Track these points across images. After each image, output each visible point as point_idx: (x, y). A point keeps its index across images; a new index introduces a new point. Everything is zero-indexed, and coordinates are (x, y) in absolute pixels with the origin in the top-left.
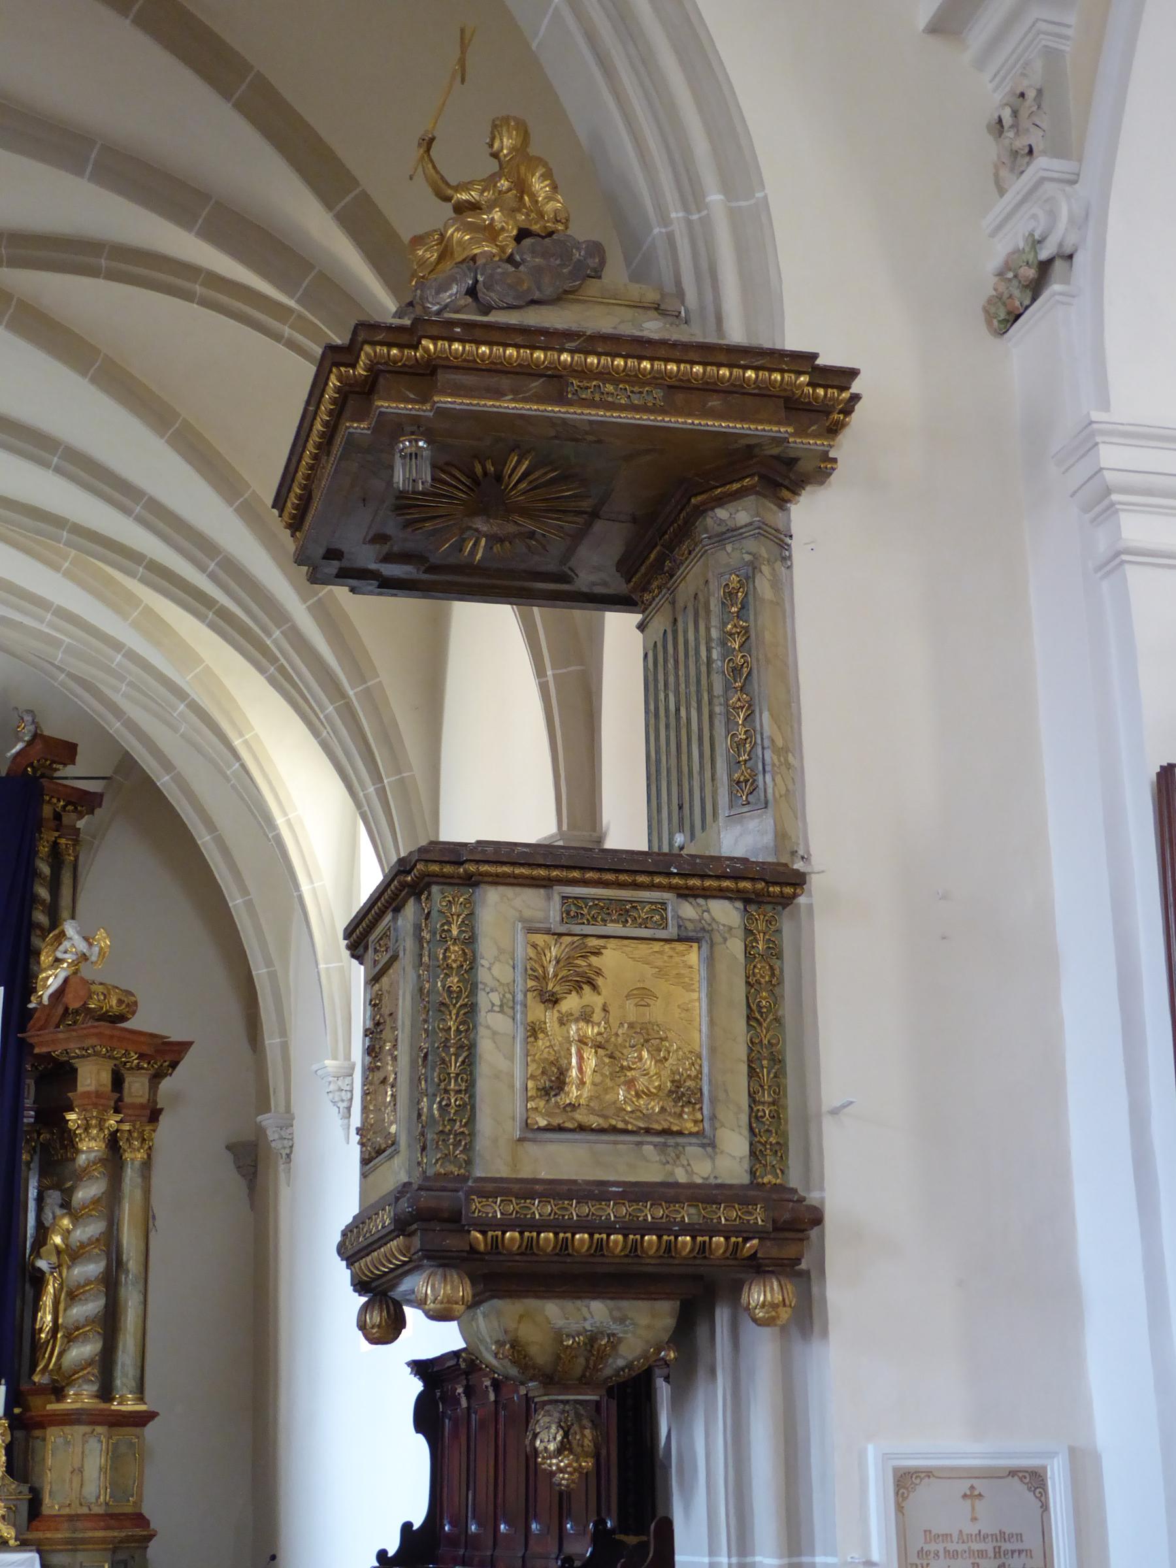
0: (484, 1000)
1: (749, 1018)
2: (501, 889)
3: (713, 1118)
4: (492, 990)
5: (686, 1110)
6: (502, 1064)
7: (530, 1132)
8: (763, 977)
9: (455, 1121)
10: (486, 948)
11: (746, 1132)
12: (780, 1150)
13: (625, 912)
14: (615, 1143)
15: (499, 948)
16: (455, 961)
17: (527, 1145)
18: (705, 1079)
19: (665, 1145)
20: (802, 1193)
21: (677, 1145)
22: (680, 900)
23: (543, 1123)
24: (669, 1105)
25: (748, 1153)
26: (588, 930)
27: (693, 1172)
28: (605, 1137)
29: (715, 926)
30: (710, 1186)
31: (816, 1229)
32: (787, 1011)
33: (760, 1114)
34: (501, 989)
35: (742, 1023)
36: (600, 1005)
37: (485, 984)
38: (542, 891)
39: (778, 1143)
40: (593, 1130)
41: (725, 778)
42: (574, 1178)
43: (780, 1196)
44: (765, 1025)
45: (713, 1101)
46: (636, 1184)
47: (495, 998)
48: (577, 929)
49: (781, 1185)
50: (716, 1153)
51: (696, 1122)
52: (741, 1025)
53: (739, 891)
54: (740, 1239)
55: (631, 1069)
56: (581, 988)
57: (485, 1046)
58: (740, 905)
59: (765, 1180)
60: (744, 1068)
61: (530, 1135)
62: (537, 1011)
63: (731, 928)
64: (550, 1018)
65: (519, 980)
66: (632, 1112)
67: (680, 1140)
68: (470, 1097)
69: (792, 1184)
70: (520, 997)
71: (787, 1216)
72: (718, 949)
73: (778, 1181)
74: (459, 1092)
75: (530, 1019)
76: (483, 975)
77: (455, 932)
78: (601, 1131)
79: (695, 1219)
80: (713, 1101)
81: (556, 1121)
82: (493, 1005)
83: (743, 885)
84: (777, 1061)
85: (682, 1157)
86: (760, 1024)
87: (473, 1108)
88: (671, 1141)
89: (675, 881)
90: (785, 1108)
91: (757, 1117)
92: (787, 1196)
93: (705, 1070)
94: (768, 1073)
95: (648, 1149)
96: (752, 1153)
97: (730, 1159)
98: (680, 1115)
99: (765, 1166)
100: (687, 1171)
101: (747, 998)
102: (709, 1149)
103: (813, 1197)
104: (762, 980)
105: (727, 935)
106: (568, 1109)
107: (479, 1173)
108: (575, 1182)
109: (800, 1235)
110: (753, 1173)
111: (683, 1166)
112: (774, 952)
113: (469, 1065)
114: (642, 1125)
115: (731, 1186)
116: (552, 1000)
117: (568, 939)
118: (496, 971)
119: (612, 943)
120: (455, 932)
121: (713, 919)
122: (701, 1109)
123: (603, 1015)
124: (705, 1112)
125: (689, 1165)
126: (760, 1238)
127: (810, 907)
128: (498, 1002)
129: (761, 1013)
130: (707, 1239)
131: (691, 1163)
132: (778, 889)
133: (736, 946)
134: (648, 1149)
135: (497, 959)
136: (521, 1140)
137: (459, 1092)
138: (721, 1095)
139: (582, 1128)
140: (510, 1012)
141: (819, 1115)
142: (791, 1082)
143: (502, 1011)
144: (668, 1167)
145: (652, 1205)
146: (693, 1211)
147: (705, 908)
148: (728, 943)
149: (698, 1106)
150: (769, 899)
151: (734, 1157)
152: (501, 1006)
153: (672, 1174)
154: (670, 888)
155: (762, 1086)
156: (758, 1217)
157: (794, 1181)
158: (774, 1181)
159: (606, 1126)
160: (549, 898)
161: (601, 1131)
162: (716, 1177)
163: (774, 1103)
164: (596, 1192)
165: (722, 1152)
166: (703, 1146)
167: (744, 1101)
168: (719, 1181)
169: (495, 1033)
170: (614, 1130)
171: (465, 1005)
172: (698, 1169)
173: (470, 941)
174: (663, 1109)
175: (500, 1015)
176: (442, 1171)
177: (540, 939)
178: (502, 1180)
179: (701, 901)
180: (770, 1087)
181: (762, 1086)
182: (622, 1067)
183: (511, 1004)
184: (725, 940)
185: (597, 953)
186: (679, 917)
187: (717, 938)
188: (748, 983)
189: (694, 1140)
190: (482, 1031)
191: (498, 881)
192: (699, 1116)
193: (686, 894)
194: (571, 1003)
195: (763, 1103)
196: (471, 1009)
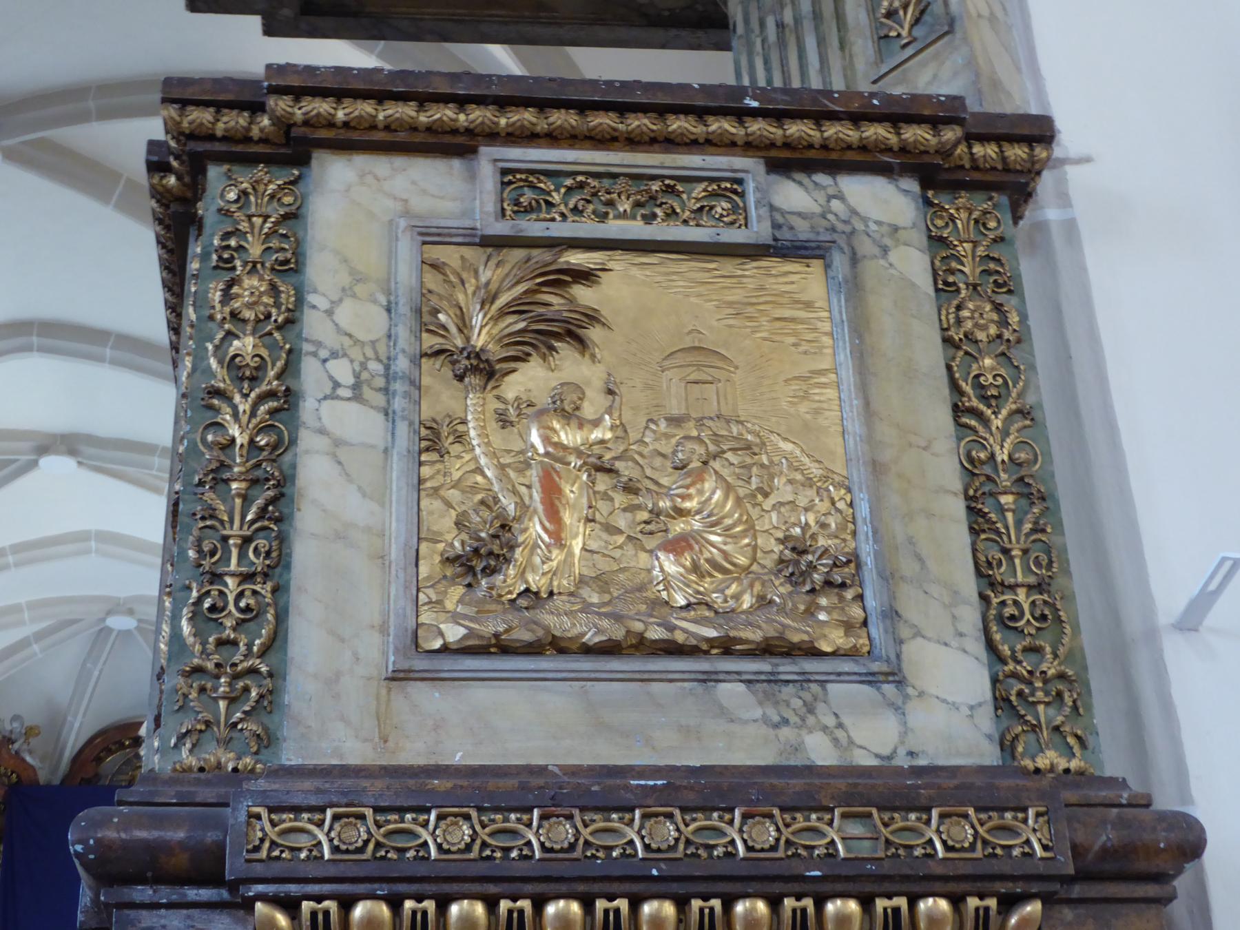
0: (311, 377)
1: (957, 410)
2: (361, 161)
3: (892, 614)
4: (334, 355)
5: (823, 601)
6: (356, 508)
7: (418, 663)
8: (984, 328)
9: (234, 643)
10: (322, 272)
11: (979, 648)
12: (1069, 688)
13: (655, 196)
14: (645, 679)
15: (353, 272)
16: (250, 306)
17: (420, 693)
18: (864, 529)
19: (773, 680)
20: (1135, 786)
21: (805, 680)
22: (774, 177)
23: (454, 633)
24: (780, 590)
25: (988, 695)
26: (561, 230)
27: (851, 742)
28: (615, 664)
29: (860, 226)
30: (899, 771)
31: (1189, 867)
32: (1044, 391)
33: (1009, 611)
34: (356, 353)
35: (942, 417)
36: (598, 383)
37: (319, 344)
38: (456, 163)
39: (1062, 676)
40: (588, 650)
41: (863, 17)
42: (539, 761)
43: (1078, 795)
44: (997, 422)
45: (888, 577)
46: (703, 770)
47: (342, 371)
48: (533, 227)
49: (1081, 773)
50: (907, 697)
51: (848, 627)
52: (937, 417)
53: (904, 150)
54: (992, 903)
55: (681, 513)
56: (552, 348)
57: (315, 471)
58: (912, 185)
59: (1042, 762)
60: (958, 507)
61: (420, 664)
62: (443, 395)
63: (896, 229)
64: (474, 407)
65: (403, 334)
66: (688, 606)
67: (810, 665)
68: (275, 591)
69: (1112, 768)
70: (402, 364)
71: (1108, 837)
72: (872, 269)
73: (1074, 764)
74: (247, 578)
75: (427, 412)
76: (314, 325)
77: (255, 251)
78: (609, 649)
79: (864, 849)
80: (888, 577)
81: (491, 627)
82: (337, 385)
83: (913, 133)
84: (1035, 493)
85: (821, 707)
86: (985, 422)
87: (281, 617)
88: (787, 668)
89: (757, 127)
90: (1069, 598)
91: (1001, 620)
92: (1105, 794)
93: (863, 509)
94: (1019, 523)
95: (731, 692)
96: (1001, 702)
97: (945, 708)
98: (810, 612)
99: (1035, 728)
100: (836, 741)
101: (949, 368)
102: (889, 689)
103: (1165, 801)
104: (981, 336)
105: (887, 241)
106: (523, 602)
107: (290, 756)
108: (542, 770)
109: (1151, 890)
110: (1007, 746)
111: (825, 729)
112: (1000, 284)
113: (278, 521)
114: (712, 633)
115: (953, 771)
116: (483, 370)
117: (519, 254)
118: (346, 314)
119: (619, 263)
120: (255, 251)
121: (854, 212)
122: (860, 597)
123: (605, 401)
124: (871, 602)
125: (840, 725)
126: (1048, 900)
127: (1071, 227)
128: (347, 379)
129: (984, 399)
130: (902, 902)
131: (846, 720)
132: (991, 150)
133: (913, 263)
134: (731, 692)
135: (347, 292)
136: (399, 677)
137: (247, 578)
138: (908, 567)
139: (558, 646)
140: (380, 399)
141: (1152, 635)
142: (1073, 539)
143: (357, 397)
144: (785, 732)
145: (746, 817)
146: (855, 829)
147: (831, 191)
148: (893, 256)
149: (849, 594)
150: (977, 176)
151: (955, 706)
152: (356, 387)
153: (797, 748)
154: (749, 147)
155: (1006, 551)
156: (1033, 837)
157: (1112, 761)
158: (1062, 764)
159: (618, 633)
160: (472, 176)
161: (609, 649)
162: (911, 754)
163: (1039, 587)
164: (603, 792)
165: (921, 694)
166: (871, 679)
167: (969, 585)
168: (922, 762)
169: (338, 443)
170: (641, 646)
171: (271, 395)
172: (861, 732)
173: (290, 267)
174: (763, 602)
175: (354, 406)
176: (193, 762)
177: (450, 256)
178: (346, 771)
179: (821, 178)
180: (1025, 552)
181: (1006, 551)
182: (656, 513)
183: (380, 382)
184: (885, 250)
185: (585, 276)
186: (772, 208)
187: (866, 247)
188: (947, 341)
189: (847, 666)
190: (307, 440)
191: (351, 140)
192: (856, 612)
193: (788, 161)
194: (530, 380)
195: (1012, 588)
196: (286, 401)
